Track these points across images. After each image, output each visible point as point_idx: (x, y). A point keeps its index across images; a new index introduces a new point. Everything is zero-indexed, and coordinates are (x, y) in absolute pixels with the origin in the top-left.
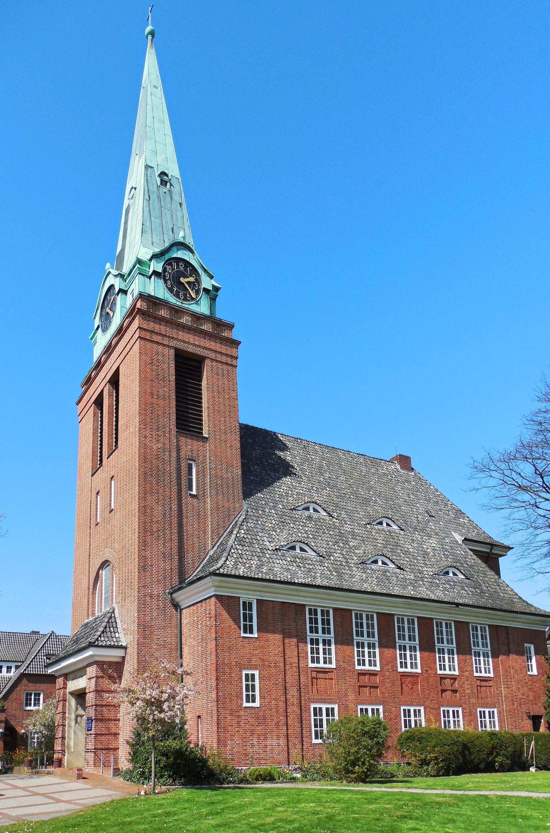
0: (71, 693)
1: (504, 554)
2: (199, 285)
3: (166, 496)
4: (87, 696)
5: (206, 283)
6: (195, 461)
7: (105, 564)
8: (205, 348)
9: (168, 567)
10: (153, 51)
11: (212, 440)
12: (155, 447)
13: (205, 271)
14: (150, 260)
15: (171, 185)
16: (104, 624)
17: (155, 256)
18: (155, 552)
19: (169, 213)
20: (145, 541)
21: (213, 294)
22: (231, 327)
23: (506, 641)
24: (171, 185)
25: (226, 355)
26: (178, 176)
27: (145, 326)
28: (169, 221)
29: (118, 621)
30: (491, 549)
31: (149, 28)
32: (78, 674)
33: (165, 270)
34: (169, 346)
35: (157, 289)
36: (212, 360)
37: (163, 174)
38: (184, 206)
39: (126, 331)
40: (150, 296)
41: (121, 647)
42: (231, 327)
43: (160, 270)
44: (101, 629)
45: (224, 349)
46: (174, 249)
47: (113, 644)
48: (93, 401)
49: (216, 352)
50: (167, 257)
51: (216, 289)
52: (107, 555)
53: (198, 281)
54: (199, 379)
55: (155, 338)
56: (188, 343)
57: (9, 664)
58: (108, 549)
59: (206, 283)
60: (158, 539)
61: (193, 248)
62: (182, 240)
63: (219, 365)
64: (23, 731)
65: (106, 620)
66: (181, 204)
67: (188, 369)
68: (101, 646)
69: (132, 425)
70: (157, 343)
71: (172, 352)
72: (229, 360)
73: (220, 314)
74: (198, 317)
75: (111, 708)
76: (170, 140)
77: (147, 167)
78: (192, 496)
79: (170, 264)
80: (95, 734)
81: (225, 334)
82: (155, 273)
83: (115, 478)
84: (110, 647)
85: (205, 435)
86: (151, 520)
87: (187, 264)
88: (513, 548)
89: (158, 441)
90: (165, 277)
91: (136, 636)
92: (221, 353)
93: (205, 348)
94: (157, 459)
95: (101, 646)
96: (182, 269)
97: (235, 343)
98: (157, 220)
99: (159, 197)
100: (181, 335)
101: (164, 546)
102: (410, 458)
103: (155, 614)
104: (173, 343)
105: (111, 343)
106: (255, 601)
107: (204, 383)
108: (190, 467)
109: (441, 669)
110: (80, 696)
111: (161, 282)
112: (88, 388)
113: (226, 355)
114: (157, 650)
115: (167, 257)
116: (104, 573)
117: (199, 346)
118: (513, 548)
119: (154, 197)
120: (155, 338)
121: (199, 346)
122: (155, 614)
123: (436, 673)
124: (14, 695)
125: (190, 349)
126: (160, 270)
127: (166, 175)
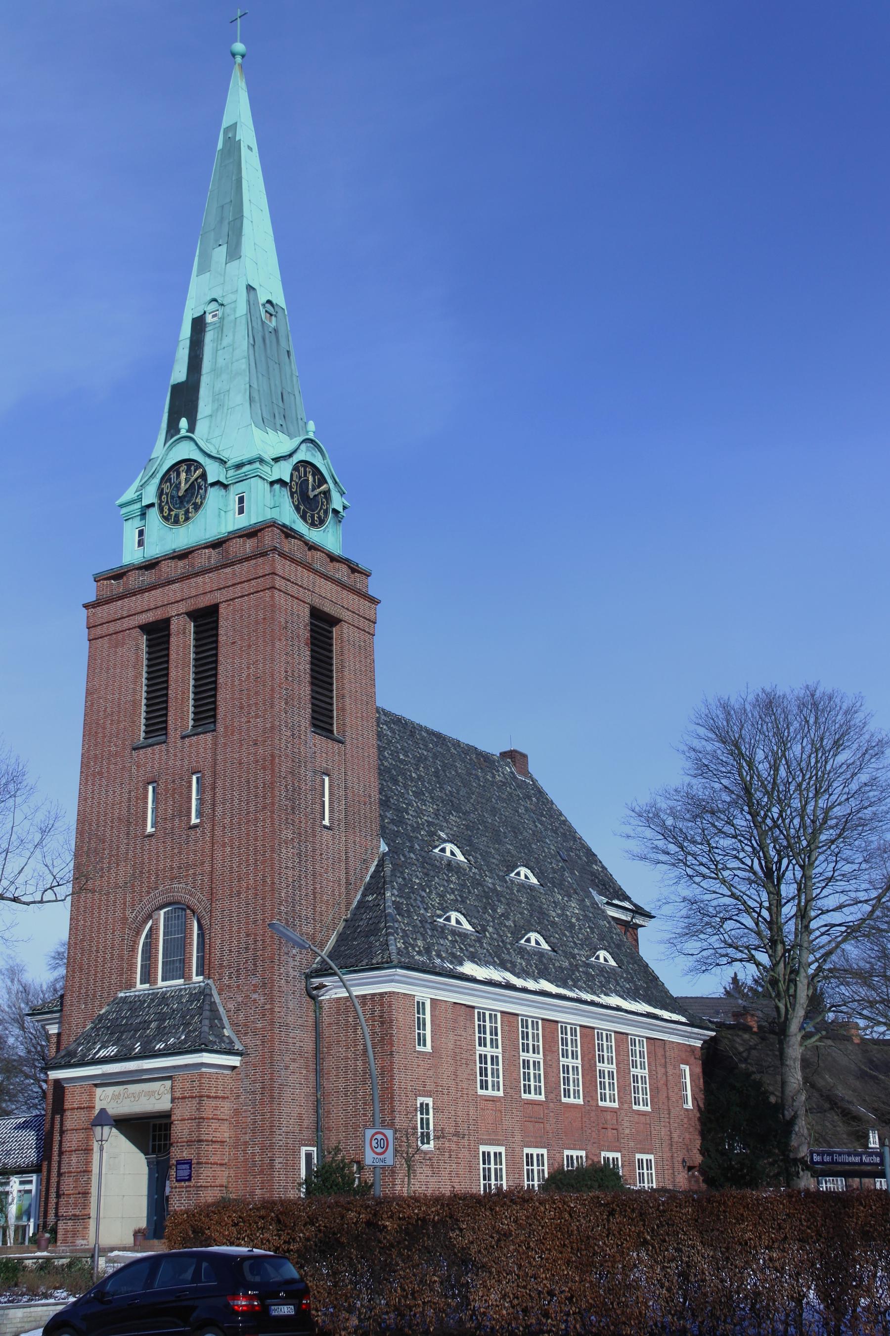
1: (104, 612)
2: (328, 503)
6: (328, 775)
10: (242, 84)
23: (663, 1061)
26: (284, 306)
30: (633, 918)
40: (284, 526)
66: (288, 352)
72: (363, 623)
78: (325, 827)
82: (280, 481)
88: (654, 917)
90: (291, 488)
97: (374, 601)
102: (524, 756)
106: (429, 1000)
109: (482, 1088)
111: (286, 493)
118: (654, 917)
123: (597, 1106)
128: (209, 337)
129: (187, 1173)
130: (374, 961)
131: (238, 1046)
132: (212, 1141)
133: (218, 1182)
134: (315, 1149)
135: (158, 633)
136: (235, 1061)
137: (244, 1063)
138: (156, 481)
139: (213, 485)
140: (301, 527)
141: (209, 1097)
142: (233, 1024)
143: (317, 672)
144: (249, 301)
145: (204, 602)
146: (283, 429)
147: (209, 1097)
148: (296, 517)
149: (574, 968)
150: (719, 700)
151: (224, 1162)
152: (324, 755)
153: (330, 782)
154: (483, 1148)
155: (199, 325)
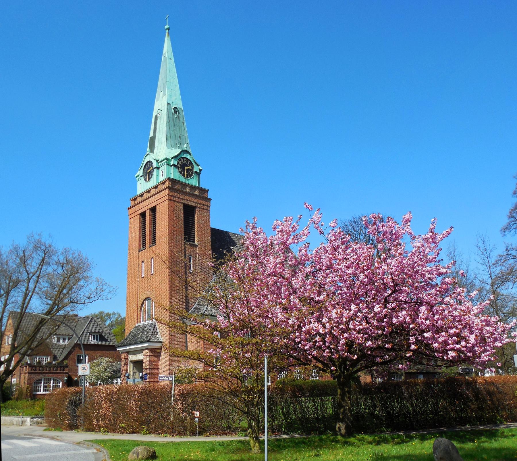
0: (131, 361)
3: (179, 272)
4: (144, 364)
5: (196, 169)
7: (147, 299)
8: (196, 203)
11: (199, 246)
13: (196, 163)
14: (172, 158)
15: (179, 113)
16: (152, 331)
17: (174, 157)
18: (176, 300)
19: (178, 128)
20: (171, 295)
21: (198, 174)
22: (207, 191)
24: (179, 113)
25: (205, 205)
27: (171, 194)
28: (178, 133)
29: (158, 329)
31: (167, 27)
32: (136, 352)
33: (178, 163)
34: (181, 203)
35: (174, 174)
36: (199, 208)
37: (175, 108)
38: (185, 124)
41: (160, 342)
42: (207, 191)
43: (176, 164)
44: (151, 333)
45: (204, 203)
46: (182, 153)
49: (201, 204)
50: (179, 157)
51: (200, 170)
52: (149, 295)
53: (193, 168)
54: (194, 217)
55: (175, 199)
56: (189, 201)
57: (64, 337)
59: (196, 169)
60: (177, 293)
61: (191, 152)
62: (185, 149)
63: (202, 210)
64: (76, 379)
65: (152, 329)
66: (183, 123)
67: (189, 212)
68: (152, 342)
70: (176, 201)
71: (182, 205)
73: (202, 186)
74: (193, 188)
76: (178, 88)
77: (168, 104)
78: (191, 273)
79: (180, 160)
81: (204, 195)
84: (156, 342)
85: (196, 243)
87: (188, 160)
89: (177, 248)
91: (168, 338)
92: (203, 205)
93: (196, 203)
95: (152, 342)
96: (185, 162)
97: (209, 200)
98: (173, 132)
99: (173, 120)
100: (186, 197)
104: (183, 201)
107: (196, 219)
108: (190, 258)
110: (138, 364)
111: (177, 170)
113: (205, 205)
114: (177, 344)
115: (179, 157)
116: (146, 302)
117: (193, 202)
119: (171, 120)
120: (175, 199)
121: (193, 202)
124: (71, 357)
125: (190, 203)
126: (176, 164)
127: (177, 108)
128: (158, 121)
130: (35, 297)
135: (143, 215)
138: (142, 168)
139: (155, 168)
140: (183, 179)
144: (167, 108)
145: (153, 205)
146: (176, 148)
148: (180, 175)
149: (390, 335)
150: (65, 249)
155: (156, 117)
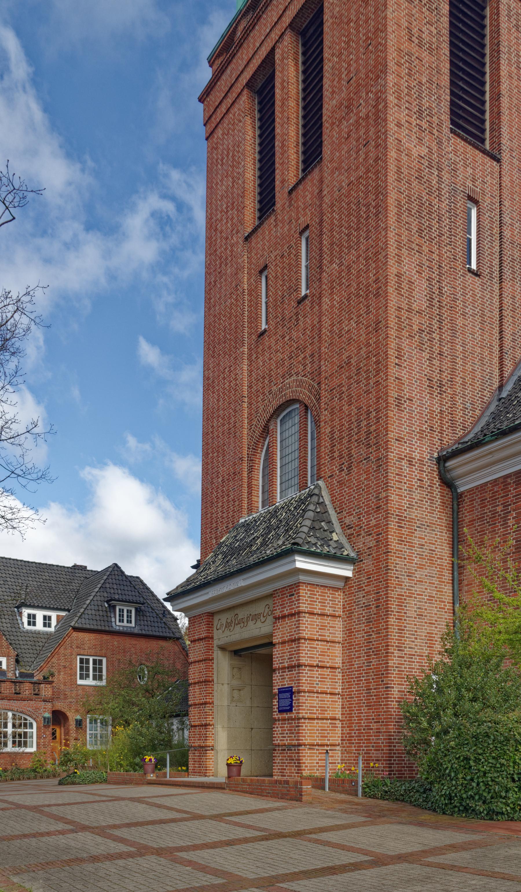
9: (436, 408)
12: (415, 152)
39: (240, 45)
47: (333, 551)
48: (245, 82)
58: (294, 377)
69: (366, 101)
75: (327, 672)
78: (470, 270)
80: (299, 719)
83: (271, 271)
86: (409, 304)
94: (419, 178)
101: (431, 365)
103: (417, 496)
105: (234, 32)
112: (229, 62)
114: (421, 567)
122: (417, 496)
129: (287, 702)
131: (348, 551)
132: (317, 666)
133: (329, 714)
134: (34, 749)
136: (347, 571)
137: (357, 572)
141: (312, 613)
142: (345, 527)
143: (461, 98)
147: (312, 613)
151: (337, 691)
152: (470, 171)
153: (478, 212)
154: (104, 660)
